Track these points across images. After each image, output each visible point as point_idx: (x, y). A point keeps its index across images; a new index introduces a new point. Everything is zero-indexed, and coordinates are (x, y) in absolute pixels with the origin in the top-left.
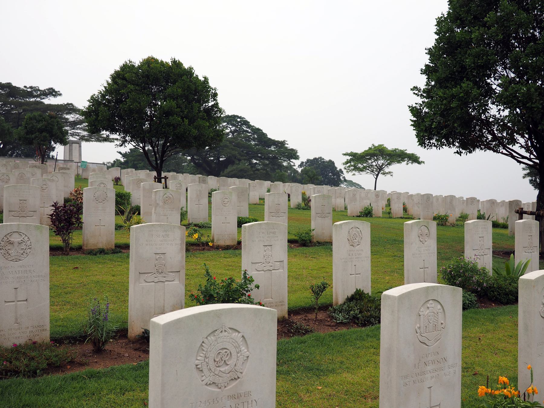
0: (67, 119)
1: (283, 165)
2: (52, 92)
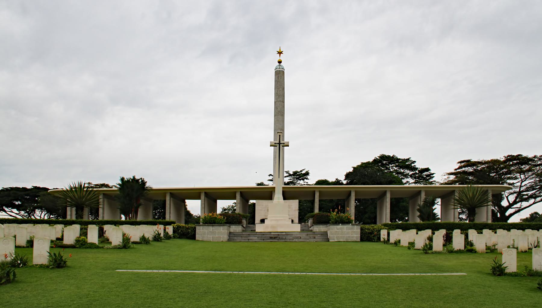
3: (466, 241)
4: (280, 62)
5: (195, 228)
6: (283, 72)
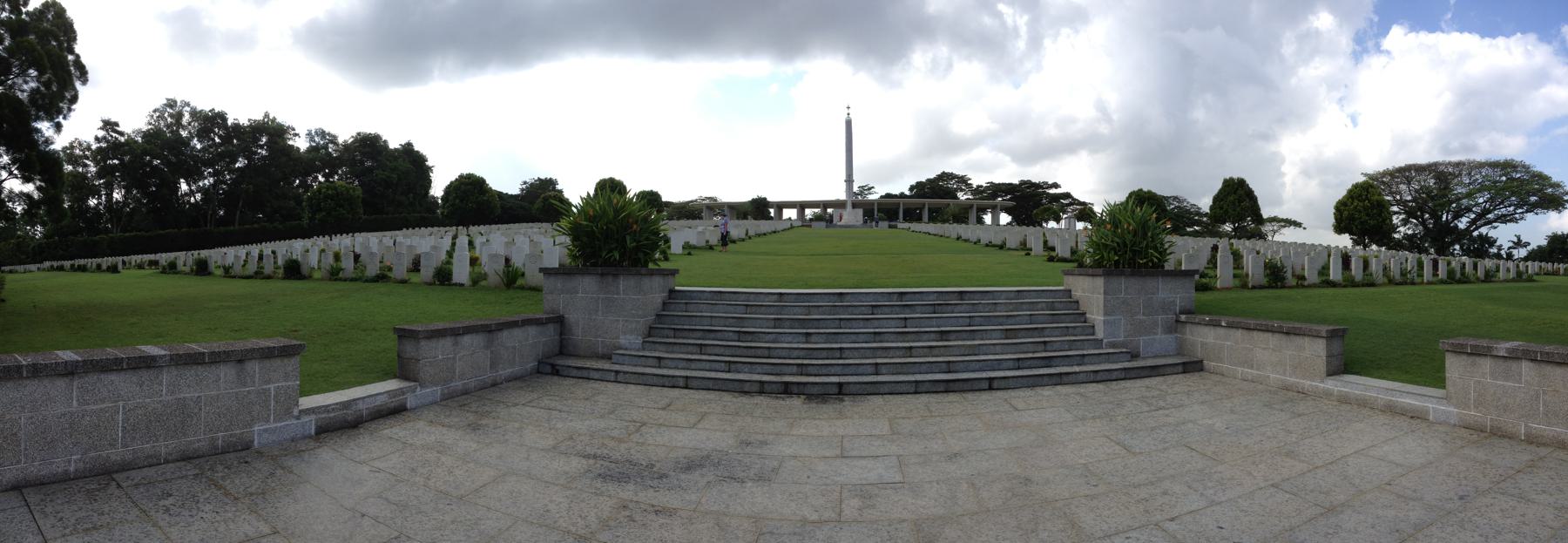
2: (1056, 186)
3: (726, 209)
4: (848, 114)
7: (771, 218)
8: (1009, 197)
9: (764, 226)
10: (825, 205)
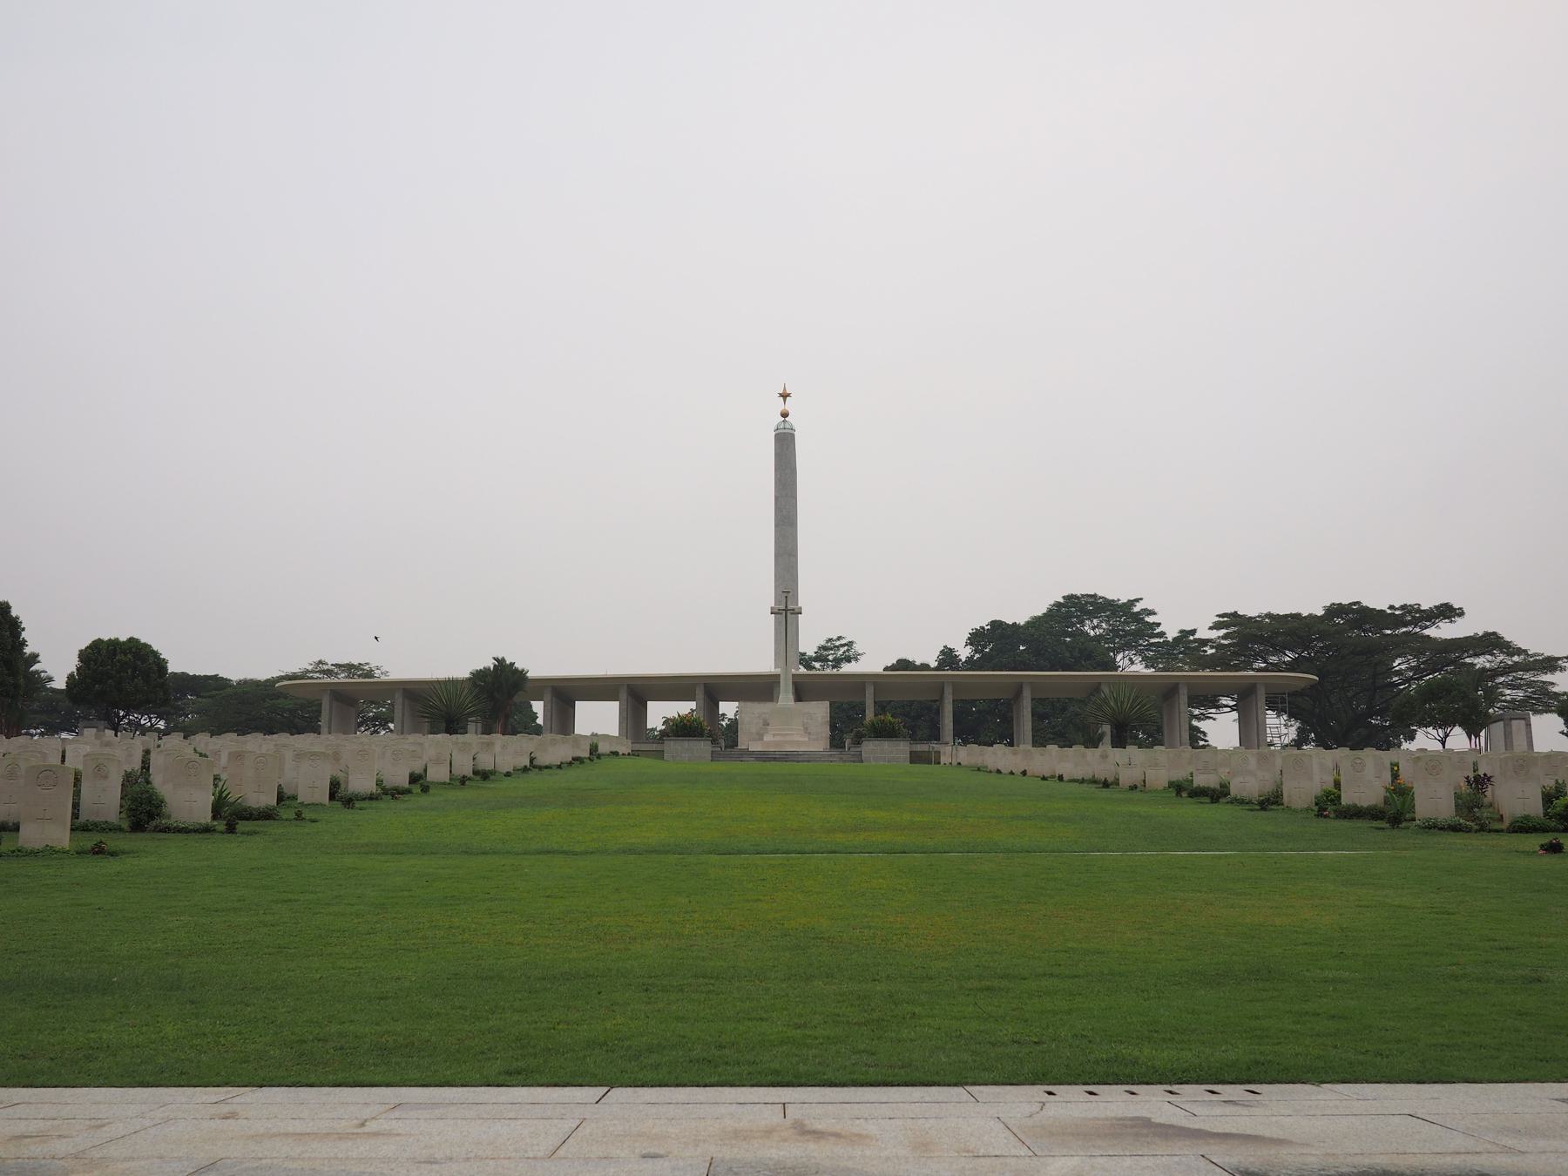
0: (1473, 665)
1: (54, 691)
2: (1447, 612)
4: (785, 415)
5: (214, 818)
6: (793, 436)
7: (538, 730)
8: (1289, 656)
9: (506, 751)
10: (712, 689)
